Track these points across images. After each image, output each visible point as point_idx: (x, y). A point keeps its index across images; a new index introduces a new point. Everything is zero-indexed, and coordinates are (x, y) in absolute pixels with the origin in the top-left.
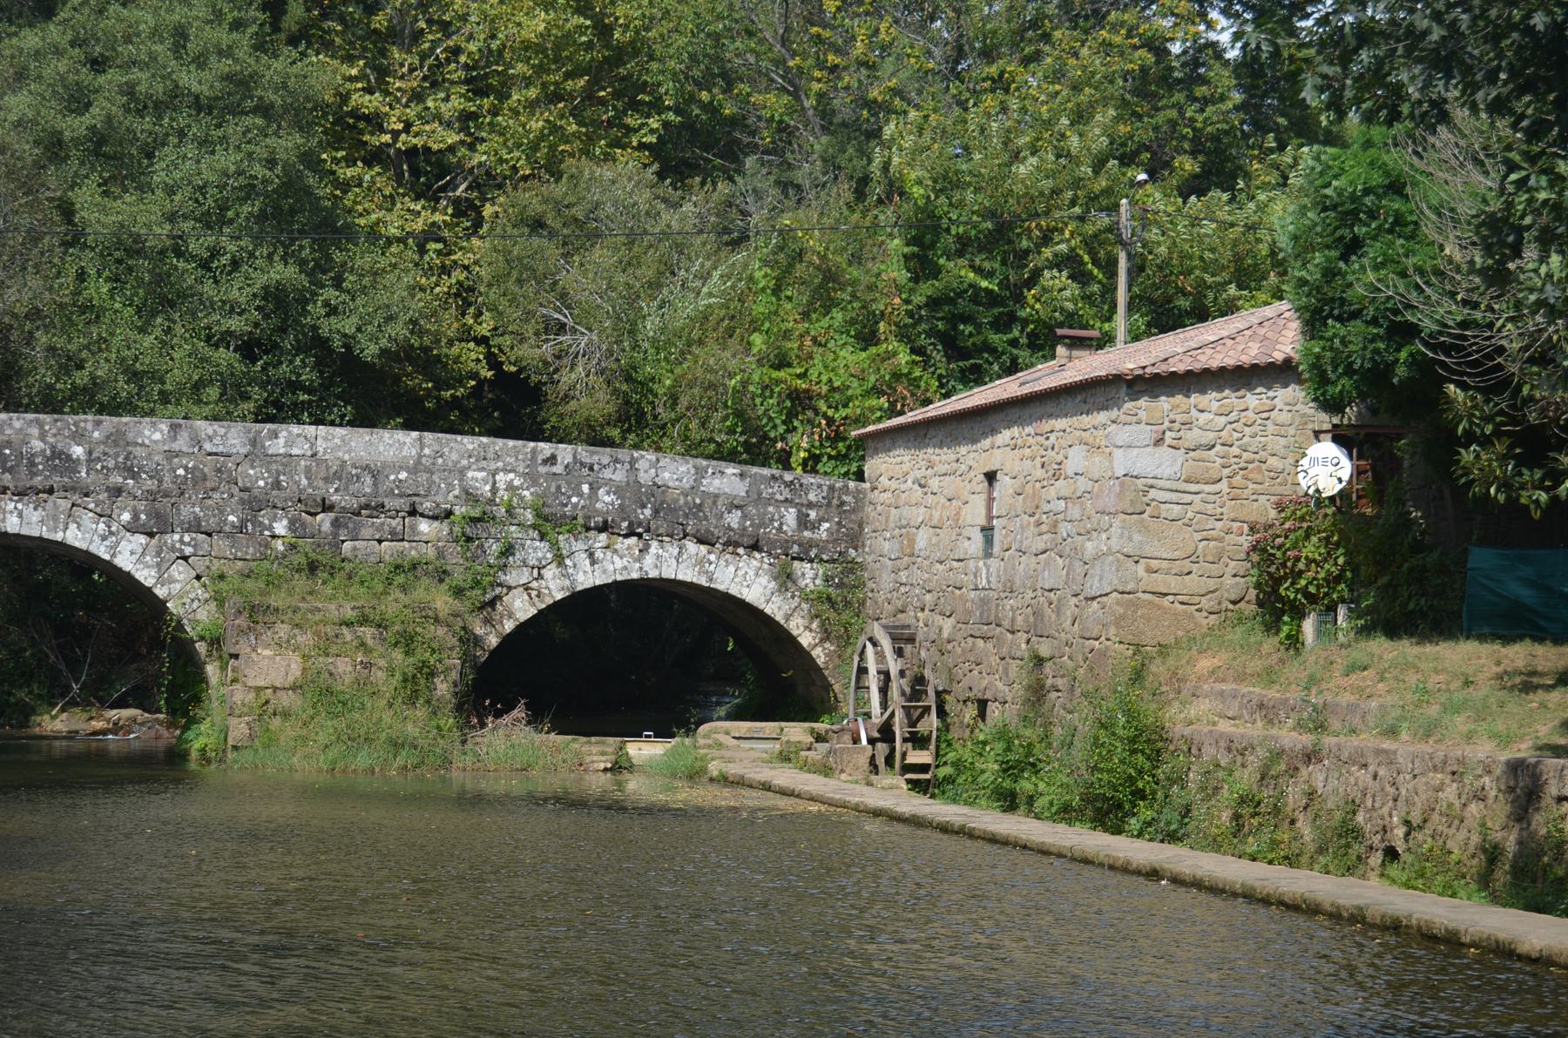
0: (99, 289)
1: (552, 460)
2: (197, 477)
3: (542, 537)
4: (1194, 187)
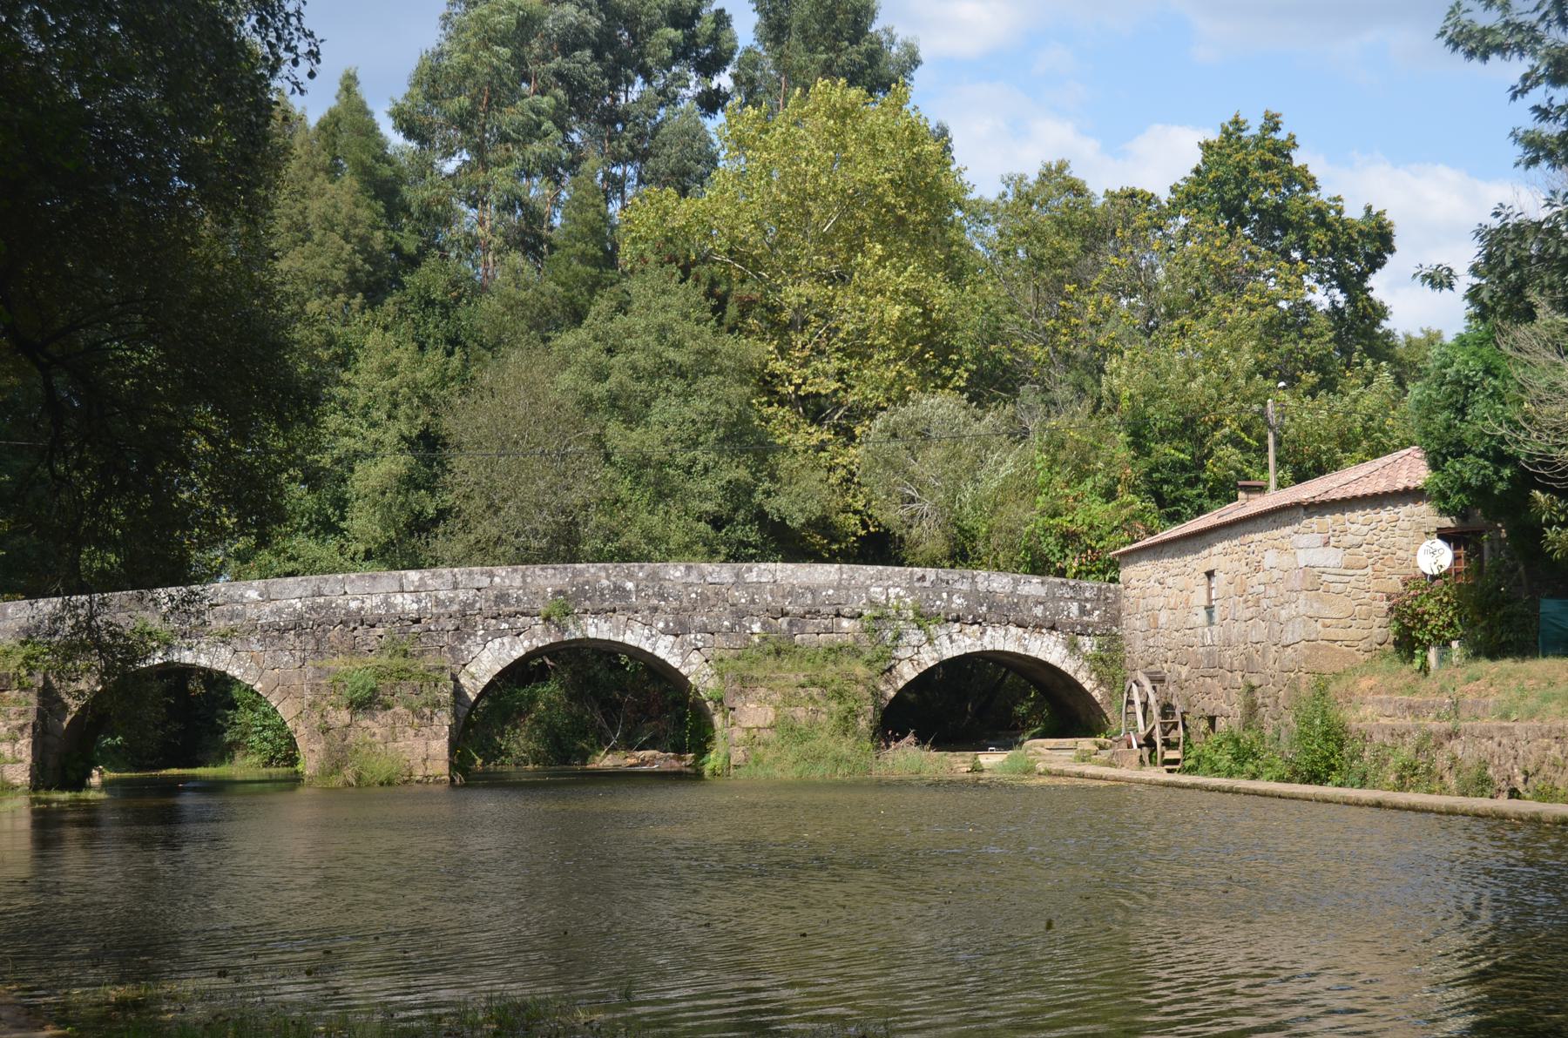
0: (623, 490)
1: (923, 578)
2: (704, 598)
3: (919, 627)
4: (1312, 393)
